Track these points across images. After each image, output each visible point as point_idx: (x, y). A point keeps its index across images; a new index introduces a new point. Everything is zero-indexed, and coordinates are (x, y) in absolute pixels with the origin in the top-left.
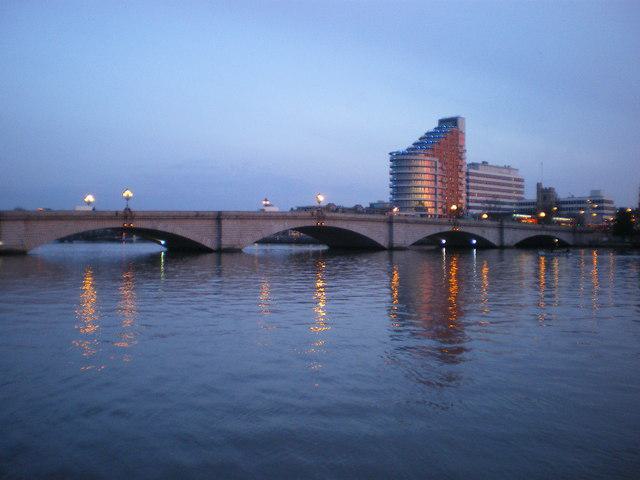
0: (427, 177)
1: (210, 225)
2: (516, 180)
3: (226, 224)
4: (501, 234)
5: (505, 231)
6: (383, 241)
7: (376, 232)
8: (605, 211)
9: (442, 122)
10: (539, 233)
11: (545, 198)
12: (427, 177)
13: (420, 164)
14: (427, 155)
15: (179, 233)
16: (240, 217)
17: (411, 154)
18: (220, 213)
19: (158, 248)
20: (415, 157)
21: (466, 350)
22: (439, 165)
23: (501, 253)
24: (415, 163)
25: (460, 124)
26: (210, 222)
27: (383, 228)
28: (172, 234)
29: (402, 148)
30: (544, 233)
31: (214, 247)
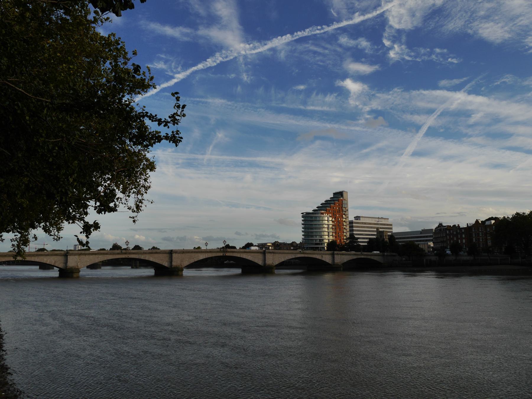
1: (166, 256)
3: (174, 255)
4: (333, 258)
5: (335, 256)
8: (359, 240)
9: (334, 194)
10: (359, 257)
15: (244, 257)
16: (183, 252)
18: (172, 250)
19: (150, 272)
21: (78, 239)
22: (330, 219)
25: (344, 195)
26: (165, 255)
28: (457, 276)
30: (363, 257)
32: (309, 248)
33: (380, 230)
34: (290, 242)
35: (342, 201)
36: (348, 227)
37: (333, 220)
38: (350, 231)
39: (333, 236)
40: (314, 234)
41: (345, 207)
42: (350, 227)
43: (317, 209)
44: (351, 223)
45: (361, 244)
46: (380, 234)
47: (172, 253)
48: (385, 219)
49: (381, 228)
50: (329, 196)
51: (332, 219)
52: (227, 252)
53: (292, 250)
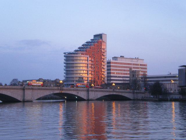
0: (84, 65)
2: (141, 65)
5: (90, 92)
6: (19, 98)
7: (16, 94)
8: (112, 78)
9: (95, 36)
10: (111, 93)
11: (133, 76)
12: (84, 65)
13: (79, 59)
14: (83, 54)
17: (76, 54)
20: (77, 55)
22: (90, 59)
23: (88, 103)
24: (77, 58)
25: (103, 37)
27: (20, 92)
29: (72, 51)
30: (115, 93)
31: (21, 100)
32: (66, 85)
33: (133, 69)
34: (53, 79)
35: (101, 43)
36: (106, 67)
37: (93, 60)
38: (108, 70)
39: (92, 75)
40: (75, 72)
41: (104, 48)
42: (108, 66)
43: (78, 49)
44: (109, 63)
45: (149, 83)
46: (133, 73)
47: (25, 89)
48: (142, 60)
49: (134, 68)
50: (90, 37)
51: (92, 58)
52: (63, 90)
53: (119, 89)
